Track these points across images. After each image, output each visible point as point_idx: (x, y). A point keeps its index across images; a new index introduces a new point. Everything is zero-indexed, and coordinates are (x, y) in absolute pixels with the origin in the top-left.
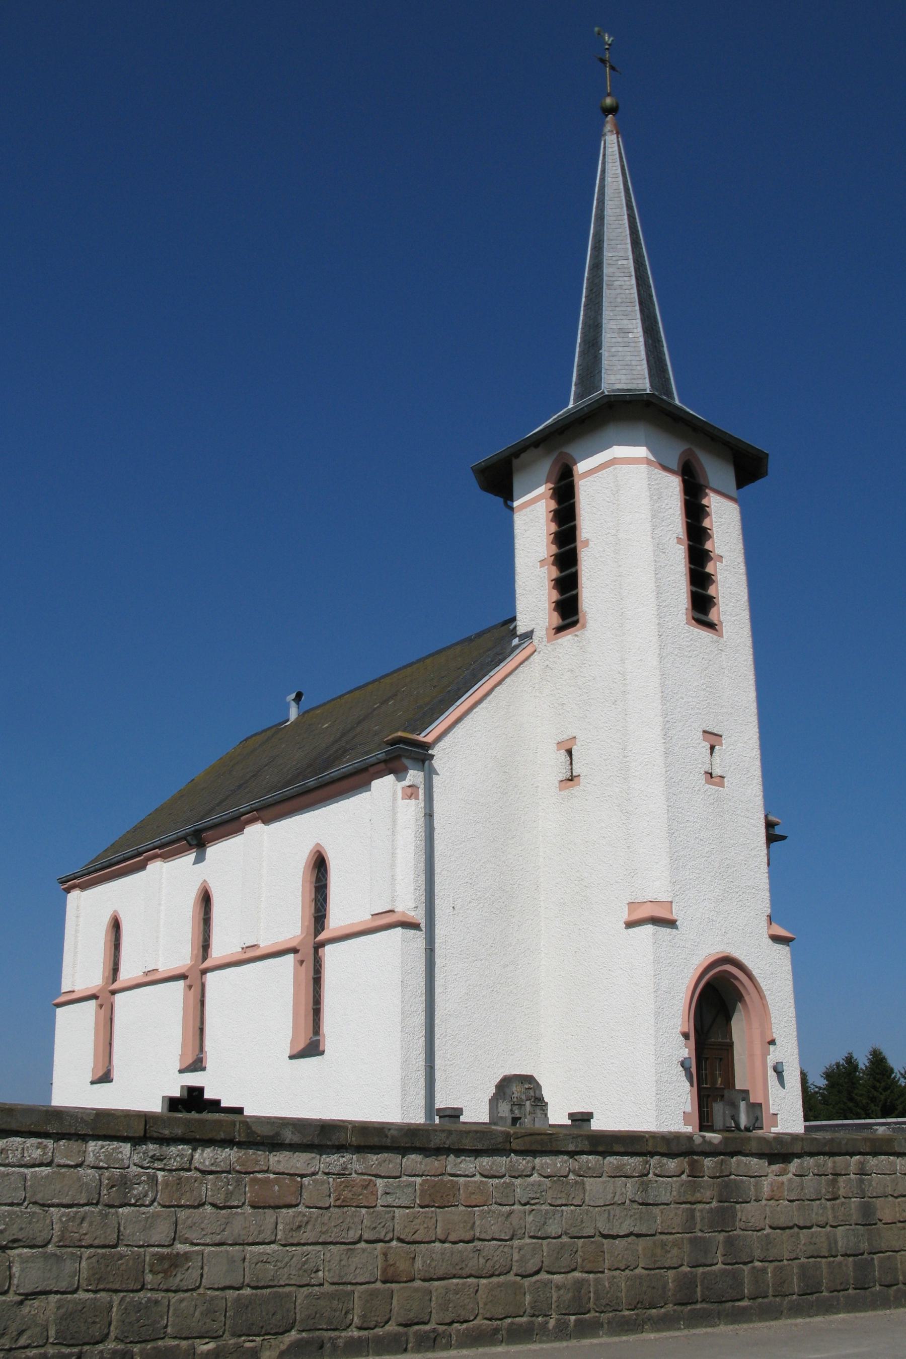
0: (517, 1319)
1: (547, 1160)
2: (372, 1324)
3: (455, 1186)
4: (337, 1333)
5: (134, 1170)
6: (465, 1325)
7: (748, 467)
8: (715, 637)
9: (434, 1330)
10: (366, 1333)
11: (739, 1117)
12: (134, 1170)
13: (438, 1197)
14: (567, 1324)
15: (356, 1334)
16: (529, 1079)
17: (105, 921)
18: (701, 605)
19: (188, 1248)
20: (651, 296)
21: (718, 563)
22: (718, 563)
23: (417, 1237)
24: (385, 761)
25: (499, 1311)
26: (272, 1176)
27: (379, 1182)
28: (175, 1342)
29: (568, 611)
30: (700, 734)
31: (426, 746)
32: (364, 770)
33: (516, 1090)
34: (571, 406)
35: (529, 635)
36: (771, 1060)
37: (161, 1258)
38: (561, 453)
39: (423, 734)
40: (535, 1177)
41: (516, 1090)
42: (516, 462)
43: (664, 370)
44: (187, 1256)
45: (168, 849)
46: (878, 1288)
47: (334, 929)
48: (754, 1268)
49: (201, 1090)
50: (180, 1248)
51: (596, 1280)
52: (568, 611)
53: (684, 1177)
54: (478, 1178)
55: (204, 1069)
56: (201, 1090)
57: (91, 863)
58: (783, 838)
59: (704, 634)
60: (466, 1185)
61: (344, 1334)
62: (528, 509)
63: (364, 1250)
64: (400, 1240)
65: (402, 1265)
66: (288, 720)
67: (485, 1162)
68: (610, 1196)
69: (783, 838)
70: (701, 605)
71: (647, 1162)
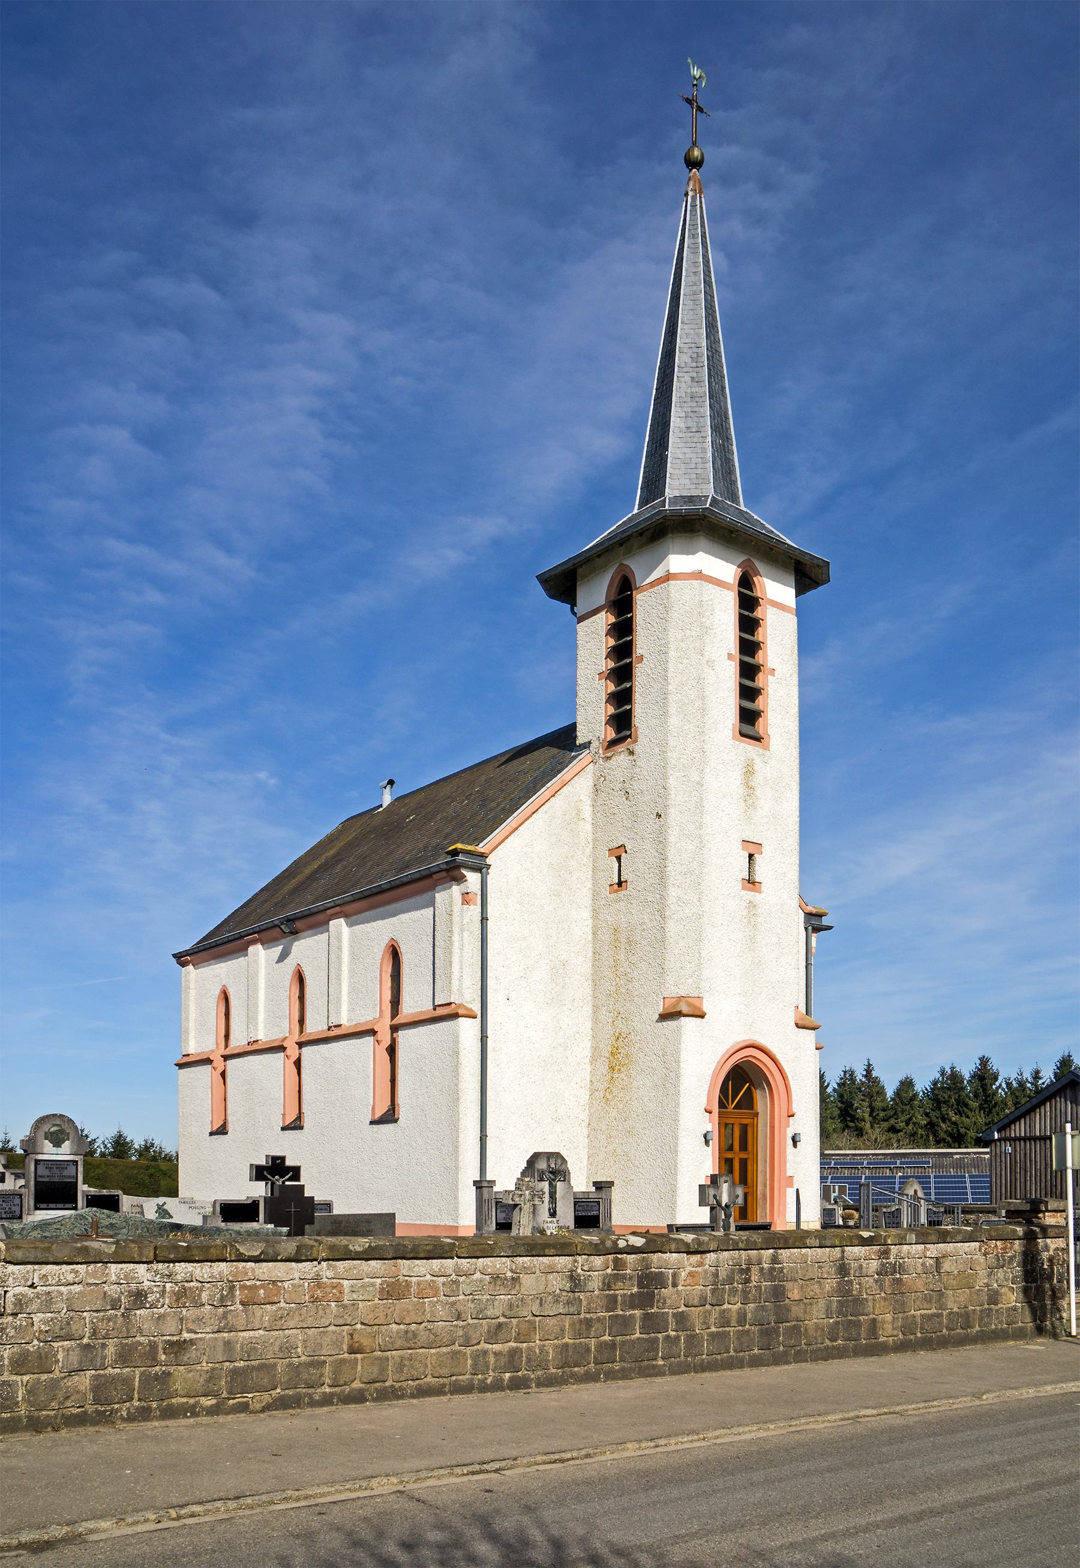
0: (460, 1377)
1: (488, 1261)
2: (342, 1382)
3: (408, 1285)
4: (313, 1390)
5: (147, 1283)
6: (418, 1382)
7: (806, 575)
8: (761, 751)
9: (392, 1386)
10: (337, 1389)
11: (721, 1197)
12: (147, 1283)
13: (394, 1291)
14: (502, 1380)
15: (328, 1390)
16: (558, 1156)
17: (217, 992)
18: (749, 717)
19: (193, 1336)
20: (723, 388)
21: (770, 677)
22: (770, 677)
23: (377, 1321)
24: (446, 870)
25: (445, 1371)
26: (259, 1283)
27: (345, 1283)
28: (184, 1400)
29: (622, 722)
30: (740, 844)
31: (484, 856)
32: (427, 876)
33: (542, 1165)
34: (636, 511)
35: (587, 745)
36: (790, 1133)
37: (172, 1344)
38: (622, 564)
39: (481, 845)
40: (478, 1275)
41: (542, 1165)
42: (580, 571)
43: (730, 471)
44: (192, 1342)
45: (267, 935)
46: (781, 1348)
47: (408, 1015)
48: (668, 1336)
49: (283, 1159)
50: (186, 1336)
51: (528, 1348)
52: (622, 722)
53: (609, 1271)
54: (429, 1277)
55: (301, 1128)
56: (283, 1159)
57: (198, 943)
58: (829, 928)
59: (748, 747)
60: (419, 1284)
61: (319, 1390)
62: (590, 620)
63: (334, 1332)
64: (362, 1323)
65: (366, 1342)
66: (381, 806)
67: (436, 1264)
68: (542, 1288)
69: (829, 928)
70: (749, 717)
71: (576, 1261)
